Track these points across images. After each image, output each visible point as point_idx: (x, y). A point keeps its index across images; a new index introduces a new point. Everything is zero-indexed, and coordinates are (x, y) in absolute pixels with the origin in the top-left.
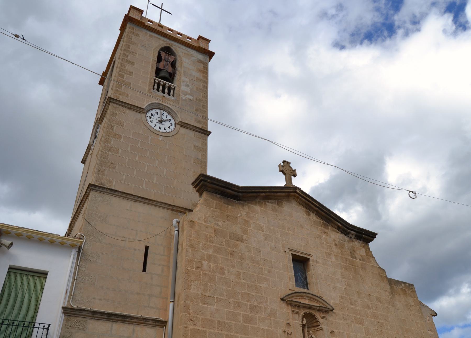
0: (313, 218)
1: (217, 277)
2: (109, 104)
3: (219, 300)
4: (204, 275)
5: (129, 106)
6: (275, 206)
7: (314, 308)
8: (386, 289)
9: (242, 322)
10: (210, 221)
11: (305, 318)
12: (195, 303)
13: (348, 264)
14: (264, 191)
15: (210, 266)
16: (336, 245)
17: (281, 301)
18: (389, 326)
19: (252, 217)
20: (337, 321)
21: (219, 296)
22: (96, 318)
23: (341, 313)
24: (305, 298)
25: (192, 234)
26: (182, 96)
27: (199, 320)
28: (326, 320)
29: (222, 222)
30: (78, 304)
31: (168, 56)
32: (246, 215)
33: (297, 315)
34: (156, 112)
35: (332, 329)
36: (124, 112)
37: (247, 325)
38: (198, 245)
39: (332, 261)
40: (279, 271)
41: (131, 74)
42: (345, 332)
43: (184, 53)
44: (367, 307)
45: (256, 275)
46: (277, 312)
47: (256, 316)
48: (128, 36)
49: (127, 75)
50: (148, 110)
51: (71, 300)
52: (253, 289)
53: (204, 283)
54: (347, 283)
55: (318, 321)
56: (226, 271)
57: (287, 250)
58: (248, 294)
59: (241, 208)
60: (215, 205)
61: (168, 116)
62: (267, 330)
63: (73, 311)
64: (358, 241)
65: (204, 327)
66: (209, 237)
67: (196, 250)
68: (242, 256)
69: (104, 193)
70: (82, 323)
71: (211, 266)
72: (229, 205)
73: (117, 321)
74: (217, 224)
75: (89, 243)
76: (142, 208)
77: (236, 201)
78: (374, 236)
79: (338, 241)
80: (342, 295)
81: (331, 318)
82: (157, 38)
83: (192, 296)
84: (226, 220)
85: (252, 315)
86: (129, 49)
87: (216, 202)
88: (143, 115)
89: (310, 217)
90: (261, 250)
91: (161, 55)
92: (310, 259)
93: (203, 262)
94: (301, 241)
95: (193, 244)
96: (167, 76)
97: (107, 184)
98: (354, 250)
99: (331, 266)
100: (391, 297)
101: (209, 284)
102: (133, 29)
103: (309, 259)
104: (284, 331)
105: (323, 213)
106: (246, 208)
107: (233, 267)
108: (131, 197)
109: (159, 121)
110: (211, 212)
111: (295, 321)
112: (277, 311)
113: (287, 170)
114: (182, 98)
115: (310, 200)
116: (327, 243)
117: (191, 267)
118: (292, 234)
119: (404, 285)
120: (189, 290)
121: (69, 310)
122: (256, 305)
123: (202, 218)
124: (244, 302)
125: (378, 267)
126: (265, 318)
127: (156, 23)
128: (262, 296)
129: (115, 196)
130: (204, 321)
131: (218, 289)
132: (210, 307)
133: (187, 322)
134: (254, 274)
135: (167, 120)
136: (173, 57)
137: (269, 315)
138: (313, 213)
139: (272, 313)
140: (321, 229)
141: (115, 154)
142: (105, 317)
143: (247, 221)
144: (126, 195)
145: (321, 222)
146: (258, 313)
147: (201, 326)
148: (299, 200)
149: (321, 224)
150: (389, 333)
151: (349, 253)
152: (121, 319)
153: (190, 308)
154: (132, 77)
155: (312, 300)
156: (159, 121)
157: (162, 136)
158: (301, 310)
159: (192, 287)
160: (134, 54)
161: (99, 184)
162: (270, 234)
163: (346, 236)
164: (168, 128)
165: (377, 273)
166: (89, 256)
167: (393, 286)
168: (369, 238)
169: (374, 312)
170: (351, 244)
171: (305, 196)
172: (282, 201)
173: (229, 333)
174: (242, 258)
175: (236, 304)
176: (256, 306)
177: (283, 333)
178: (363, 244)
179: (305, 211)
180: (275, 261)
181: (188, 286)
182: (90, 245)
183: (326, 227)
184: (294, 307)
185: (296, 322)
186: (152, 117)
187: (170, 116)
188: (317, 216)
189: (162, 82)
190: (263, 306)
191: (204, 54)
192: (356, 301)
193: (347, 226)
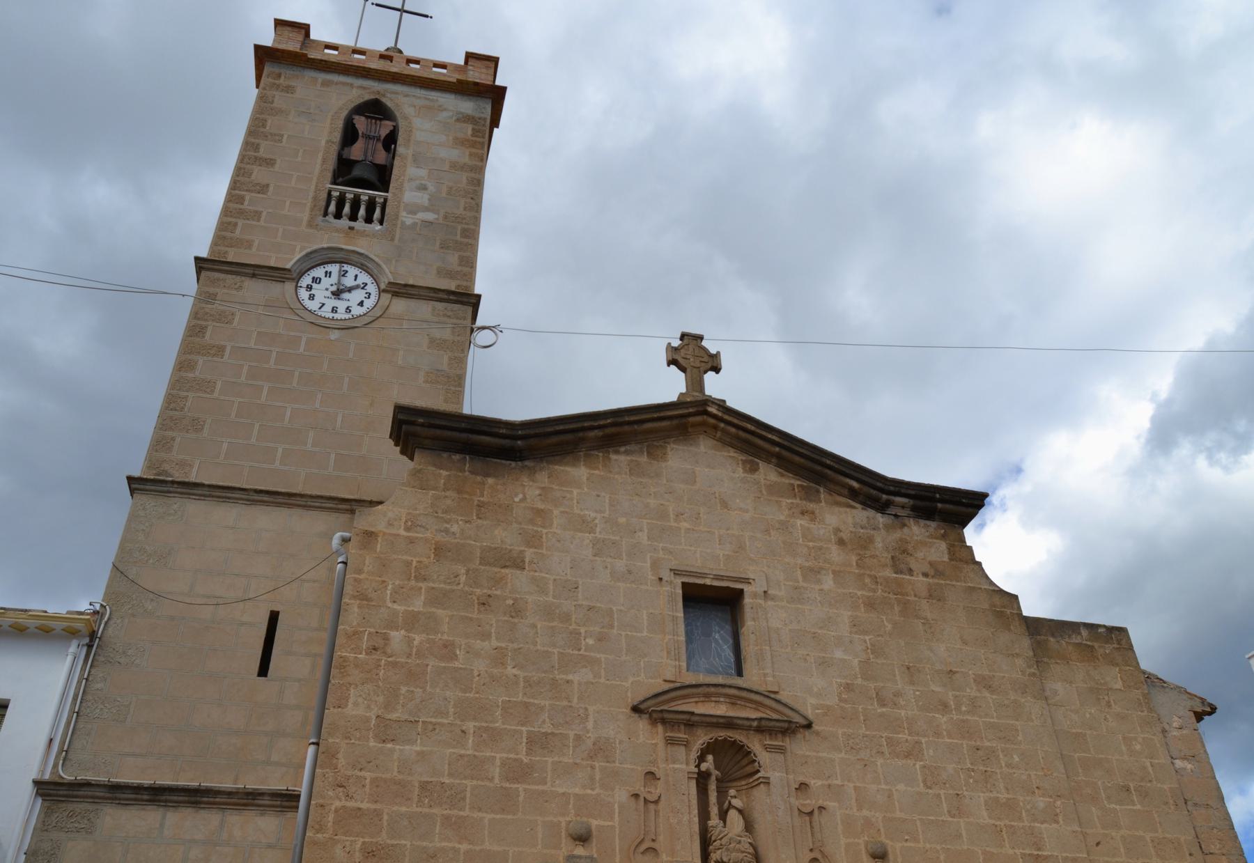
0: (768, 478)
1: (429, 667)
2: (201, 272)
3: (430, 727)
4: (390, 667)
5: (250, 271)
6: (639, 459)
7: (743, 725)
8: (1017, 651)
9: (497, 781)
10: (424, 524)
11: (709, 754)
12: (357, 742)
13: (880, 591)
14: (596, 424)
15: (410, 641)
16: (841, 542)
17: (633, 715)
18: (1015, 756)
19: (561, 499)
20: (824, 755)
21: (431, 717)
22: (122, 802)
23: (840, 732)
24: (717, 699)
25: (364, 564)
26: (403, 216)
27: (363, 783)
28: (782, 756)
29: (460, 523)
30: (78, 772)
31: (376, 123)
32: (540, 495)
33: (683, 748)
34: (326, 272)
35: (801, 779)
36: (236, 286)
37: (512, 786)
38: (379, 592)
39: (822, 590)
40: (635, 634)
41: (263, 189)
42: (851, 785)
43: (417, 108)
44: (940, 707)
45: (556, 651)
46: (618, 745)
47: (546, 761)
48: (263, 97)
49: (253, 194)
50: (303, 271)
51: (61, 762)
52: (542, 691)
53: (388, 686)
54: (869, 647)
55: (755, 761)
56: (460, 650)
57: (666, 575)
59: (526, 480)
60: (443, 481)
61: (358, 277)
62: (576, 795)
63: (61, 788)
64: (922, 522)
65: (376, 802)
66: (416, 567)
67: (374, 605)
68: (516, 604)
69: (166, 495)
70: (86, 815)
71: (416, 643)
72: (487, 475)
73: (177, 805)
74: (447, 531)
75: (118, 621)
76: (268, 520)
77: (513, 464)
78: (976, 502)
79: (851, 532)
80: (849, 682)
81: (799, 747)
82: (344, 84)
83: (349, 724)
84: (475, 518)
85: (533, 758)
86: (262, 130)
87: (447, 473)
88: (289, 286)
89: (755, 476)
90: (580, 583)
91: (354, 124)
92: (745, 590)
93: (391, 632)
94: (719, 544)
95: (365, 589)
96: (370, 176)
97: (177, 471)
98: (905, 551)
99: (819, 605)
100: (1033, 670)
101: (404, 689)
102: (279, 76)
103: (742, 591)
104: (636, 796)
105: (797, 459)
106: (543, 478)
107: (486, 636)
109: (333, 293)
110: (430, 502)
111: (671, 766)
112: (617, 742)
113: (688, 357)
114: (403, 223)
115: (753, 428)
116: (811, 541)
117: (352, 649)
118: (689, 529)
119: (1090, 633)
120: (340, 709)
121: (52, 787)
122: (549, 731)
123: (401, 520)
124: (508, 727)
125: (994, 591)
126: (576, 764)
127: (348, 47)
128: (571, 707)
129: (197, 498)
130: (377, 786)
131: (431, 699)
132: (402, 747)
133: (327, 790)
134: (550, 650)
135: (357, 287)
136: (387, 122)
137: (588, 754)
138: (769, 462)
139: (601, 750)
140: (792, 503)
141: (204, 395)
142: (146, 797)
143: (542, 510)
144: (225, 491)
145: (792, 485)
146: (552, 751)
147: (366, 800)
148: (719, 434)
149: (794, 489)
150: (1015, 775)
151: (889, 562)
152: (186, 799)
153: (340, 756)
154: (265, 196)
155: (739, 702)
156: (333, 293)
157: (339, 329)
158: (698, 733)
159: (351, 700)
160: (277, 138)
161: (156, 474)
162: (614, 538)
163: (882, 513)
164: (358, 305)
165: (986, 606)
166: (117, 651)
167: (1046, 638)
168: (963, 509)
169: (963, 721)
170: (897, 534)
171: (735, 421)
172: (665, 443)
173: (455, 812)
174: (516, 610)
175: (484, 735)
176: (550, 734)
177: (633, 799)
178: (943, 528)
179: (742, 460)
180: (622, 608)
181: (337, 700)
182: (120, 626)
183: (809, 495)
184: (673, 726)
185: (677, 766)
186: (314, 285)
187: (366, 274)
188: (780, 470)
189: (350, 192)
190: (571, 734)
191: (478, 96)
192: (897, 694)
193: (879, 484)
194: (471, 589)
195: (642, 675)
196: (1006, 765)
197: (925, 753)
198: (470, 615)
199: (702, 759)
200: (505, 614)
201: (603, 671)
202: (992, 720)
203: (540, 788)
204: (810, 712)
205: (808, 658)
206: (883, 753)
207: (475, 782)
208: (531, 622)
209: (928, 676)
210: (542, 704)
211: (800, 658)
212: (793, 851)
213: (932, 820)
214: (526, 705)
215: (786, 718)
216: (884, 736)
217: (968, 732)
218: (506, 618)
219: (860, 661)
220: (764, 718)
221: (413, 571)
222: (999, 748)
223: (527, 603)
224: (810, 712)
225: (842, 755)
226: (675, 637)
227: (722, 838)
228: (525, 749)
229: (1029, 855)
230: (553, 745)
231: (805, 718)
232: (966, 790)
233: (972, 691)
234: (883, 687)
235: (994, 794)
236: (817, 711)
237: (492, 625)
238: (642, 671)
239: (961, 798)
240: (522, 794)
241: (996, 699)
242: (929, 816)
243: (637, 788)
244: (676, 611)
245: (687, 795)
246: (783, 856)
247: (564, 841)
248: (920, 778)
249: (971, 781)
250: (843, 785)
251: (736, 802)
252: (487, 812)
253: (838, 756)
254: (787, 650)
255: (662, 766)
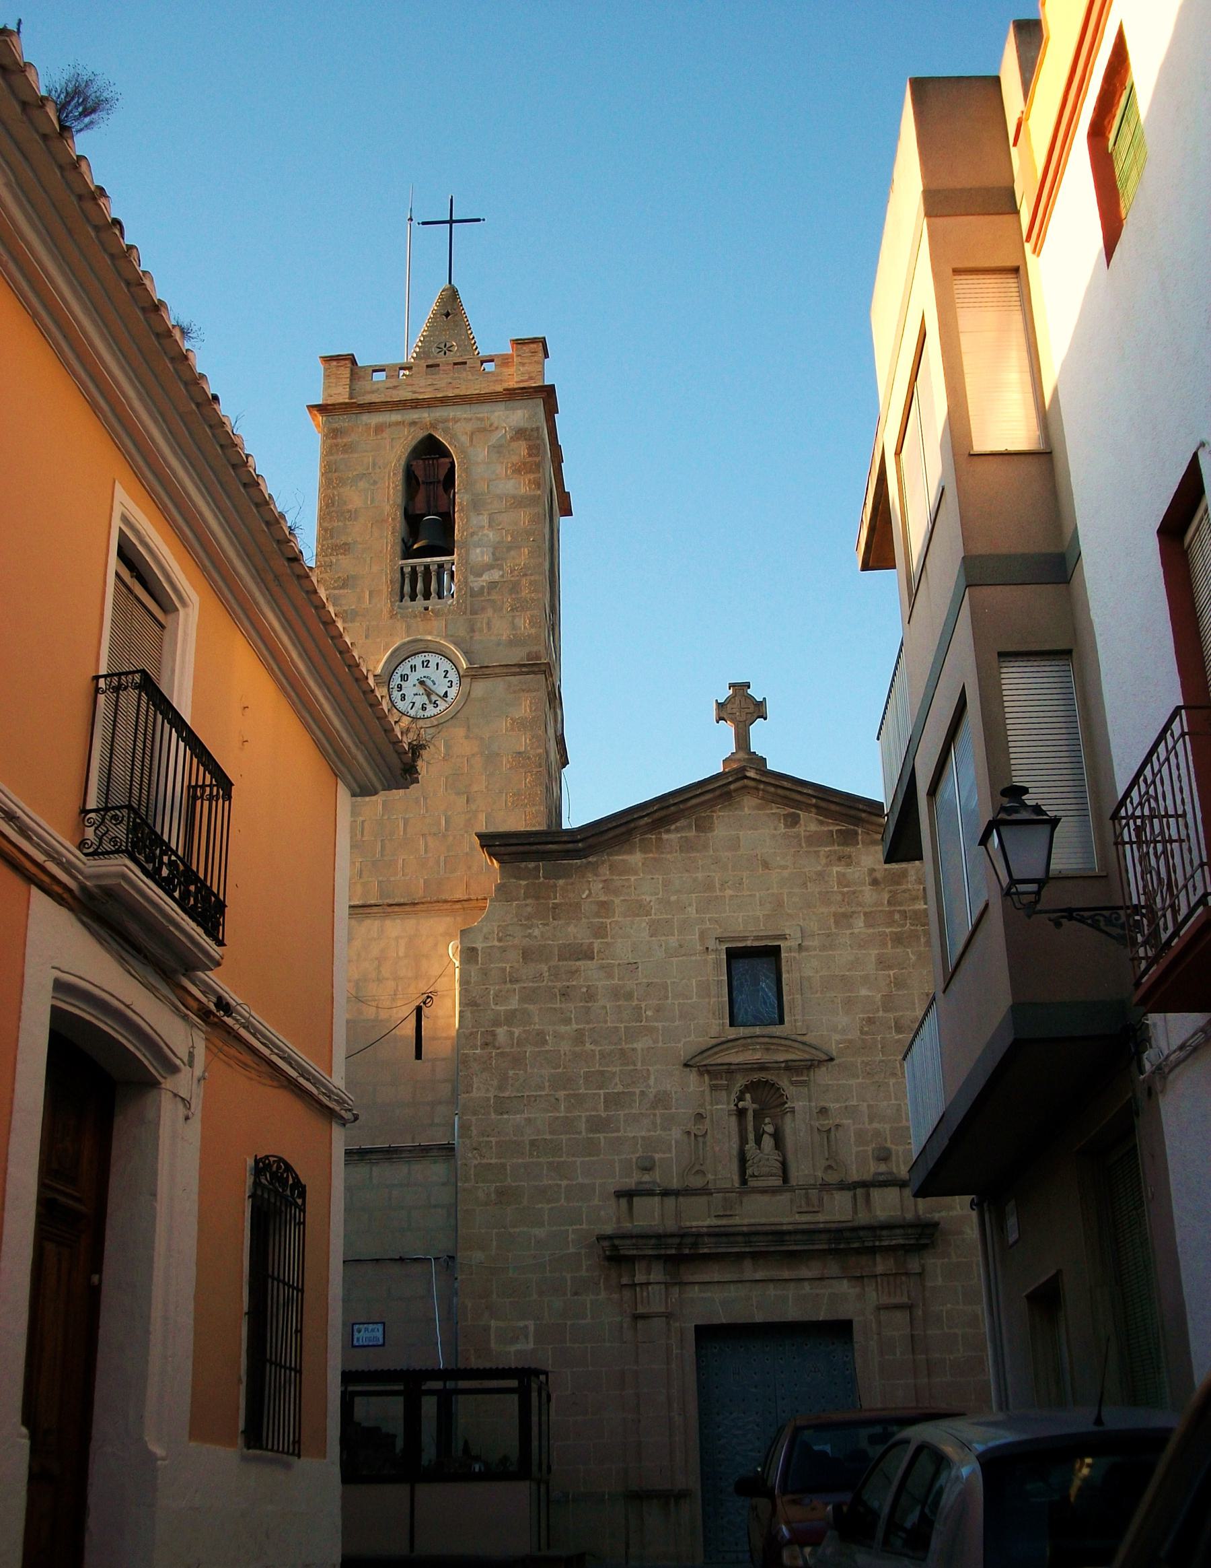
9: (584, 1134)
15: (511, 1033)
42: (865, 1104)
57: (712, 944)
58: (602, 1073)
60: (522, 891)
71: (516, 1035)
101: (511, 1073)
104: (688, 1133)
107: (567, 1021)
108: (376, 911)
153: (473, 1128)
159: (475, 1086)
190: (637, 1091)
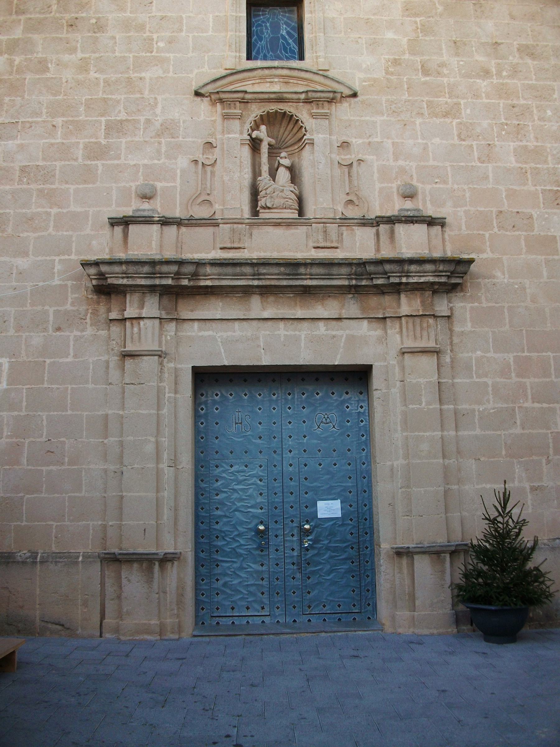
1: (27, 80)
3: (28, 125)
9: (80, 160)
15: (11, 62)
20: (368, 118)
21: (28, 118)
24: (272, 80)
35: (345, 139)
40: (201, 34)
42: (390, 141)
44: (482, 74)
45: (131, 55)
56: (51, 64)
62: (145, 166)
71: (16, 63)
80: (397, 57)
101: (7, 99)
104: (196, 161)
107: (73, 50)
111: (226, 136)
112: (181, 122)
122: (124, 119)
126: (145, 141)
128: (143, 98)
131: (28, 104)
132: (5, 143)
134: (126, 55)
150: (546, 127)
155: (291, 81)
175: (70, 127)
177: (193, 164)
190: (142, 119)
192: (442, 65)
194: (61, 15)
195: (206, 66)
196: (538, 119)
197: (463, 112)
198: (60, 36)
199: (256, 127)
200: (89, 31)
201: (171, 67)
202: (530, 82)
203: (116, 162)
204: (357, 84)
205: (359, 40)
206: (422, 114)
207: (63, 163)
208: (111, 35)
209: (474, 49)
210: (119, 98)
211: (352, 41)
212: (331, 195)
213: (463, 166)
214: (105, 100)
215: (330, 89)
216: (425, 100)
217: (506, 93)
218: (90, 34)
219: (409, 39)
220: (310, 91)
221: (14, 8)
222: (534, 105)
223: (107, 20)
224: (357, 84)
225: (385, 118)
226: (237, 34)
227: (267, 188)
228: (103, 133)
229: (549, 190)
230: (126, 128)
231: (350, 88)
232: (498, 141)
233: (514, 59)
234: (429, 60)
235: (524, 143)
236: (364, 83)
237: (77, 41)
238: (206, 64)
239: (492, 147)
240: (100, 168)
241: (536, 65)
242: (460, 162)
243: (197, 156)
244: (240, 12)
245: (239, 158)
246: (321, 200)
247: (133, 200)
248: (455, 132)
249: (504, 133)
250: (382, 142)
251: (282, 161)
252: (72, 184)
253: (379, 119)
254: (340, 35)
255: (219, 136)
